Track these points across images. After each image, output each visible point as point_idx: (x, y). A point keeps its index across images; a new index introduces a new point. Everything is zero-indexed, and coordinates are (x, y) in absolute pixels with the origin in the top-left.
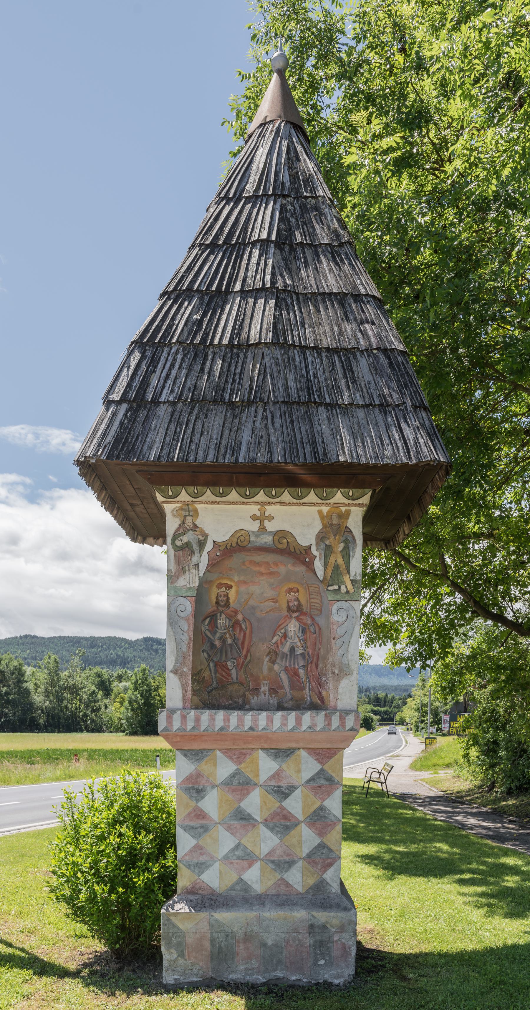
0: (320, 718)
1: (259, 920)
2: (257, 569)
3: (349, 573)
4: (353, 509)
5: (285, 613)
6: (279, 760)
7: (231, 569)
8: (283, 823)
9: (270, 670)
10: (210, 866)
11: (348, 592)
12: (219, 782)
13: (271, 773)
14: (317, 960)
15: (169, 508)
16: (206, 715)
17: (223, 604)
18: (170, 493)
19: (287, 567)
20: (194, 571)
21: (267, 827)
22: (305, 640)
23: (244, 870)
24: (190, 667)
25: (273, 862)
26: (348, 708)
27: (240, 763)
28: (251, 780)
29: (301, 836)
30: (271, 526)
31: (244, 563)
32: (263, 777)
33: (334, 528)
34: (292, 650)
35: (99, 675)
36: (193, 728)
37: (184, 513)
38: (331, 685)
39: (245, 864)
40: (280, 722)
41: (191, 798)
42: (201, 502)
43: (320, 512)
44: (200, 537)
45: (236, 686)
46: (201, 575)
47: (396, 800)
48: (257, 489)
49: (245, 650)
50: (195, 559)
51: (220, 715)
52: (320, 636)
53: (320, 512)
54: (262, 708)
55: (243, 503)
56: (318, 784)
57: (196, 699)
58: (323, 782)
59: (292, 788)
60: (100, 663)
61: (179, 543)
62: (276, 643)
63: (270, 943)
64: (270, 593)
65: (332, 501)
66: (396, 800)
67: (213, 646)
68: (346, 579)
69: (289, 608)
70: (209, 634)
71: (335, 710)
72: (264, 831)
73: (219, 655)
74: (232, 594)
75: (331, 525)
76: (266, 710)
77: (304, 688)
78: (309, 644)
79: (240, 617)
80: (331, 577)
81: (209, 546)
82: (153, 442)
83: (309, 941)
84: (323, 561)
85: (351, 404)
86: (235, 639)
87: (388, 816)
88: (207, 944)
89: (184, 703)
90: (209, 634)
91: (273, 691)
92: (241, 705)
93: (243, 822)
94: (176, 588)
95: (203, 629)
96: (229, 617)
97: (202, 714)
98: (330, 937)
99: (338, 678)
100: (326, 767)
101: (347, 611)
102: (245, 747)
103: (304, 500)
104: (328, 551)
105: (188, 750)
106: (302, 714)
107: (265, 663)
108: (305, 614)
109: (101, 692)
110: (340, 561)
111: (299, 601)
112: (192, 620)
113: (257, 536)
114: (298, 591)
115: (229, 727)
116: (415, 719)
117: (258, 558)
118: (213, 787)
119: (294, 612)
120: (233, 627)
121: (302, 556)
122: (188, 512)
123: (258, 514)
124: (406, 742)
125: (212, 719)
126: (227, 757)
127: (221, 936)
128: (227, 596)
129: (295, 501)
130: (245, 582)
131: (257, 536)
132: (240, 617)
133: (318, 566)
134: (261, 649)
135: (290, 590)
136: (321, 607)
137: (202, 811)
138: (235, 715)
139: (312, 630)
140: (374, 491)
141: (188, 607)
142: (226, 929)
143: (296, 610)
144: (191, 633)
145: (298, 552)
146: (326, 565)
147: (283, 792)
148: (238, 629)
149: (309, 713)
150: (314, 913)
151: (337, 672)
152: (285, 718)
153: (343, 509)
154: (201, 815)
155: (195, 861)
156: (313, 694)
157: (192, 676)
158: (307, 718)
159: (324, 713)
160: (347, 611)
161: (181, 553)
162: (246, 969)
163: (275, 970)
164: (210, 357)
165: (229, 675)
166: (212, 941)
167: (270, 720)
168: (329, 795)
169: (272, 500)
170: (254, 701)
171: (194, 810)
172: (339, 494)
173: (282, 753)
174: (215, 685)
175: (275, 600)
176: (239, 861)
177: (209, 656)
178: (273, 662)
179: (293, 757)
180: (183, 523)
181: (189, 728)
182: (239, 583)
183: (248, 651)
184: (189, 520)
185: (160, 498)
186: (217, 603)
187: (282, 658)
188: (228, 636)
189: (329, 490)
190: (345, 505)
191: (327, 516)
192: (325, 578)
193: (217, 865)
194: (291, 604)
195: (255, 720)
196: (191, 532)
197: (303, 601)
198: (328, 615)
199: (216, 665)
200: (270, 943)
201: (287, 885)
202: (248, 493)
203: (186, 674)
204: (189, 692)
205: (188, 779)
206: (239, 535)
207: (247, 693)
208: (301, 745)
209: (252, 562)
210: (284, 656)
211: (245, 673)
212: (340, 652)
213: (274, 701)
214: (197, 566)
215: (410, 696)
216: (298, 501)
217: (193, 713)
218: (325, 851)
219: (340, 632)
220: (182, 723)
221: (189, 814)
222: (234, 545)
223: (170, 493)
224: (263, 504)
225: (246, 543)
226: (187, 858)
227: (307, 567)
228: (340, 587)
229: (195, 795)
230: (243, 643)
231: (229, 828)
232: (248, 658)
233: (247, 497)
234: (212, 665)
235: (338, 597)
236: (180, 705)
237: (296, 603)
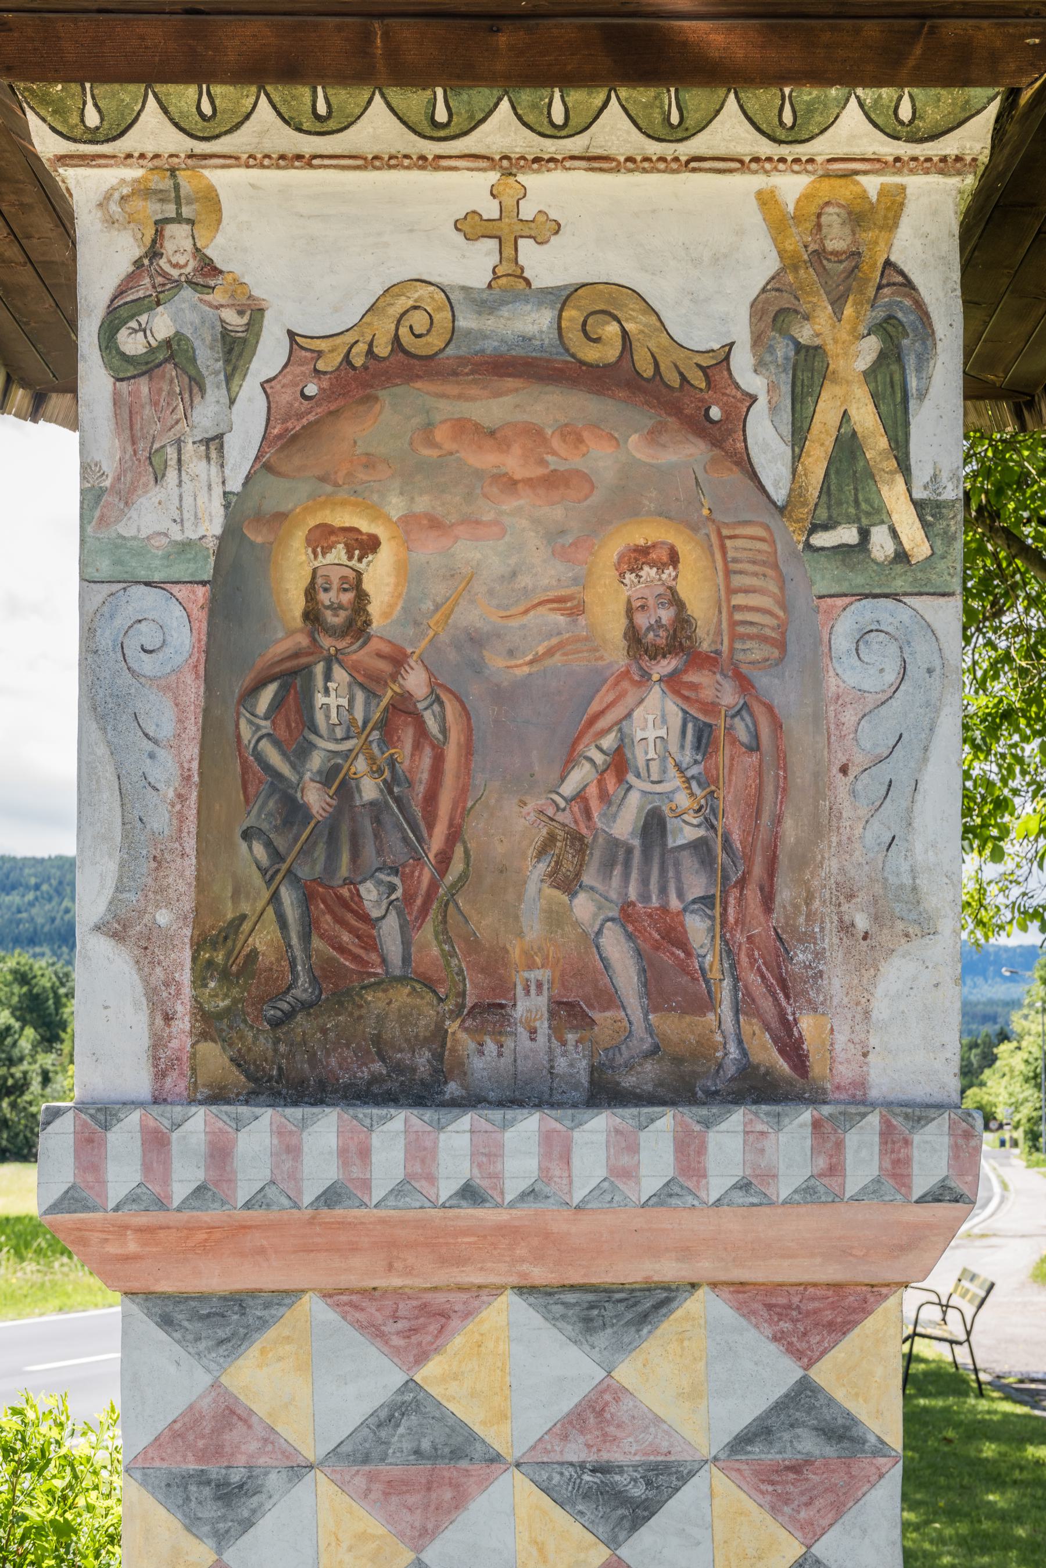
0: (790, 1142)
2: (488, 460)
3: (905, 468)
4: (915, 183)
6: (602, 1339)
7: (370, 462)
9: (556, 919)
13: (567, 1404)
15: (85, 186)
16: (259, 1131)
17: (340, 619)
18: (92, 118)
19: (622, 448)
20: (197, 466)
24: (188, 904)
26: (920, 1092)
27: (422, 1358)
28: (472, 1437)
30: (545, 265)
31: (428, 428)
33: (831, 263)
34: (654, 825)
35: (22, 977)
36: (200, 1190)
37: (154, 210)
38: (836, 983)
40: (599, 1169)
41: (192, 1524)
42: (231, 160)
43: (766, 200)
44: (231, 317)
45: (401, 996)
46: (235, 485)
47: (1007, 1407)
48: (480, 96)
49: (440, 831)
50: (206, 414)
51: (325, 1130)
52: (781, 760)
53: (766, 200)
54: (519, 1095)
55: (422, 162)
56: (789, 1457)
57: (215, 1057)
58: (809, 1444)
59: (665, 1477)
60: (32, 940)
61: (132, 343)
62: (580, 796)
64: (547, 574)
65: (821, 147)
66: (1007, 1407)
67: (293, 811)
68: (894, 496)
69: (633, 636)
70: (274, 758)
71: (859, 1101)
73: (320, 852)
74: (379, 576)
75: (819, 255)
76: (538, 1106)
77: (707, 1003)
78: (728, 797)
79: (415, 681)
80: (826, 489)
84: (787, 416)
86: (394, 781)
87: (997, 1480)
89: (160, 1075)
90: (274, 758)
91: (568, 1013)
92: (424, 1087)
95: (246, 732)
96: (368, 683)
97: (239, 1124)
99: (867, 949)
100: (823, 1374)
101: (903, 643)
102: (443, 1276)
103: (697, 145)
104: (807, 372)
105: (180, 1299)
106: (707, 1124)
107: (532, 888)
108: (709, 661)
109: (30, 1032)
110: (865, 417)
111: (676, 601)
112: (193, 691)
114: (674, 559)
115: (366, 1184)
116: (1026, 1111)
117: (497, 406)
119: (656, 653)
120: (386, 728)
121: (687, 399)
122: (174, 201)
123: (490, 209)
124: (1005, 1186)
125: (290, 1149)
126: (360, 1327)
128: (356, 585)
129: (655, 149)
130: (435, 524)
132: (415, 681)
133: (765, 437)
134: (510, 826)
135: (638, 557)
136: (782, 628)
138: (393, 1131)
140: (1013, 94)
141: (175, 627)
144: (192, 751)
145: (674, 380)
146: (799, 435)
148: (408, 736)
149: (738, 1117)
151: (862, 922)
152: (627, 1144)
153: (872, 184)
156: (751, 1027)
157: (198, 946)
158: (729, 1138)
159: (807, 1115)
160: (903, 643)
161: (143, 386)
165: (371, 944)
167: (557, 1151)
168: (839, 1510)
169: (550, 147)
170: (483, 1059)
172: (852, 116)
174: (303, 990)
177: (276, 856)
180: (154, 252)
181: (180, 1191)
182: (411, 526)
183: (455, 836)
184: (178, 241)
185: (46, 143)
186: (312, 616)
188: (361, 765)
189: (808, 94)
190: (877, 164)
191: (797, 219)
192: (796, 494)
194: (642, 620)
195: (487, 1154)
196: (187, 292)
197: (699, 602)
198: (814, 671)
199: (307, 898)
202: (441, 116)
203: (168, 940)
204: (183, 1023)
205: (177, 1434)
206: (403, 303)
207: (452, 1026)
208: (705, 1268)
209: (463, 427)
210: (616, 854)
211: (443, 933)
212: (878, 831)
213: (573, 1062)
215: (1004, 1037)
216: (667, 149)
217: (199, 1122)
219: (873, 737)
220: (147, 1168)
222: (383, 349)
223: (92, 118)
224: (509, 165)
225: (435, 342)
227: (716, 443)
228: (865, 534)
229: (211, 1510)
230: (431, 798)
232: (457, 867)
233: (435, 131)
234: (288, 897)
235: (859, 580)
236: (138, 1082)
237: (666, 615)
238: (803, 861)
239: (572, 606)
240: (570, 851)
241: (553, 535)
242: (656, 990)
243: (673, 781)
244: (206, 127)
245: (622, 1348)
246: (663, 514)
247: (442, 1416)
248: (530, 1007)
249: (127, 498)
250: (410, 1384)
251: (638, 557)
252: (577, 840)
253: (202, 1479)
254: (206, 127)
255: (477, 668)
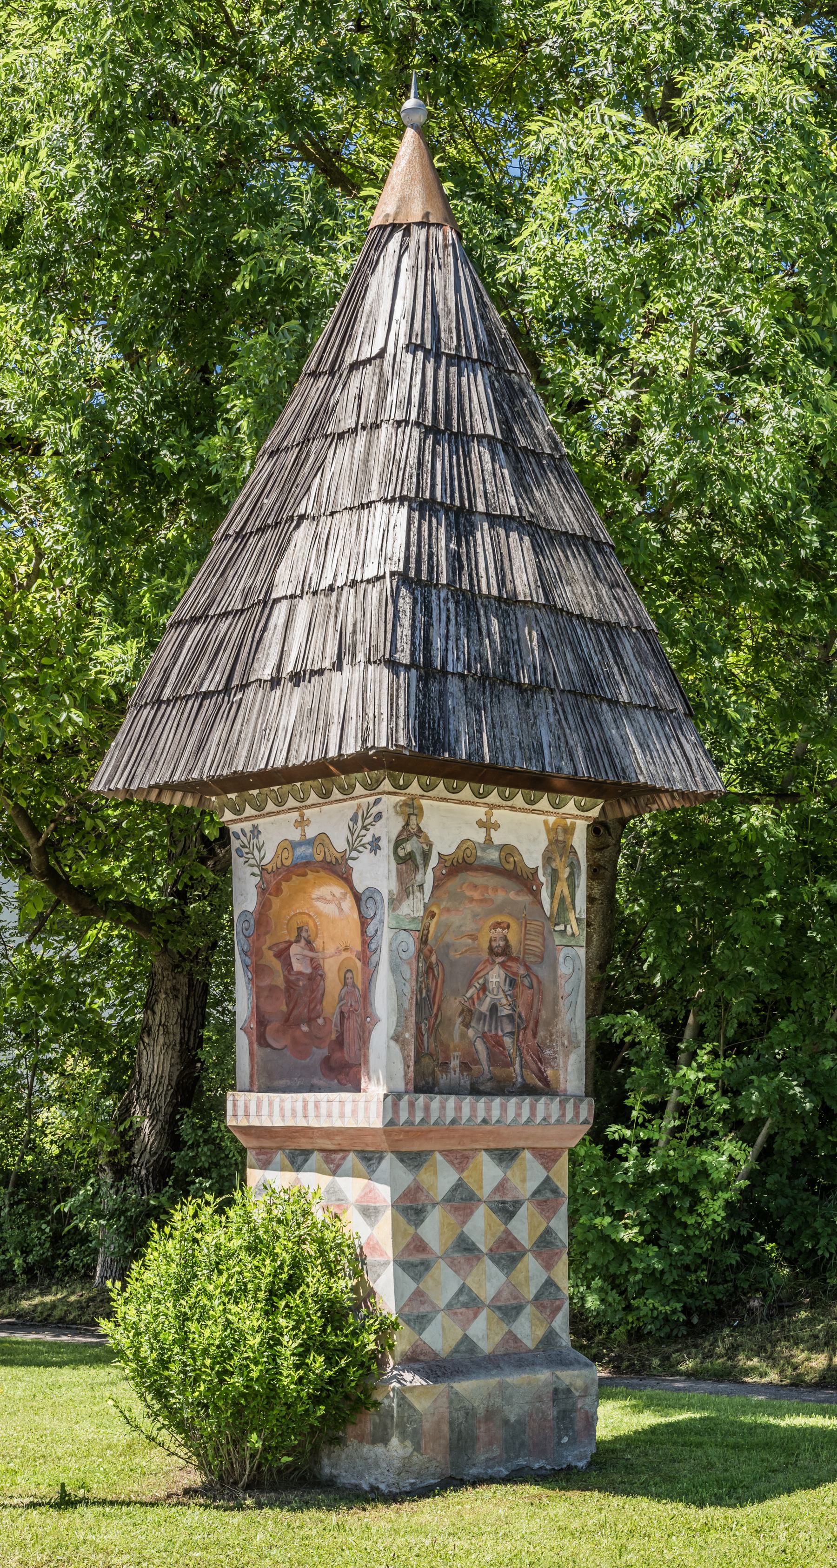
1: (502, 1387)
5: (485, 955)
8: (508, 1254)
9: (463, 1036)
10: (432, 1319)
11: (573, 934)
12: (440, 1199)
14: (560, 1438)
19: (510, 894)
20: (418, 894)
21: (492, 1259)
22: (514, 997)
23: (469, 1322)
25: (499, 1308)
29: (527, 1271)
30: (498, 838)
32: (486, 1190)
33: (559, 845)
34: (494, 1008)
39: (470, 1313)
42: (430, 798)
43: (546, 823)
50: (419, 877)
52: (541, 992)
53: (546, 823)
54: (454, 1090)
58: (549, 1194)
61: (401, 853)
62: (471, 998)
63: (513, 1419)
68: (572, 917)
69: (491, 949)
72: (488, 1265)
77: (512, 1064)
78: (520, 1002)
81: (434, 861)
82: (458, 732)
83: (552, 1413)
85: (630, 703)
88: (445, 1428)
91: (465, 1066)
93: (467, 1255)
94: (398, 916)
97: (432, 1099)
98: (574, 1404)
104: (554, 876)
105: (406, 1153)
108: (516, 960)
110: (566, 892)
113: (484, 850)
114: (508, 927)
118: (434, 1205)
119: (498, 955)
121: (525, 880)
127: (461, 1415)
128: (505, 939)
131: (484, 850)
132: (433, 959)
135: (498, 925)
136: (543, 953)
137: (422, 1240)
139: (526, 982)
142: (467, 1404)
143: (502, 953)
147: (506, 1210)
150: (558, 1373)
152: (519, 1107)
154: (420, 1246)
155: (415, 1313)
158: (542, 1103)
161: (404, 867)
162: (488, 1460)
163: (517, 1457)
164: (482, 612)
166: (451, 1423)
170: (443, 1080)
171: (413, 1239)
172: (571, 803)
173: (506, 1156)
175: (474, 937)
176: (463, 1310)
178: (467, 1025)
179: (518, 1161)
180: (407, 824)
181: (418, 1120)
183: (439, 1008)
187: (479, 1020)
193: (439, 1317)
194: (494, 944)
200: (513, 1419)
201: (516, 1340)
205: (405, 1195)
213: (466, 1081)
214: (421, 886)
218: (553, 1290)
221: (408, 1245)
224: (492, 807)
226: (406, 1309)
231: (452, 1265)
235: (564, 941)
237: (502, 943)
238: (550, 1023)
239: (474, 937)
240: (468, 1014)
241: (475, 916)
242: (493, 1059)
243: (501, 995)
244: (427, 788)
245: (508, 1167)
246: (510, 914)
247: (468, 1188)
248: (455, 1063)
249: (400, 902)
250: (460, 1179)
251: (498, 925)
252: (470, 1011)
253: (411, 1208)
254: (427, 788)
255: (447, 955)
